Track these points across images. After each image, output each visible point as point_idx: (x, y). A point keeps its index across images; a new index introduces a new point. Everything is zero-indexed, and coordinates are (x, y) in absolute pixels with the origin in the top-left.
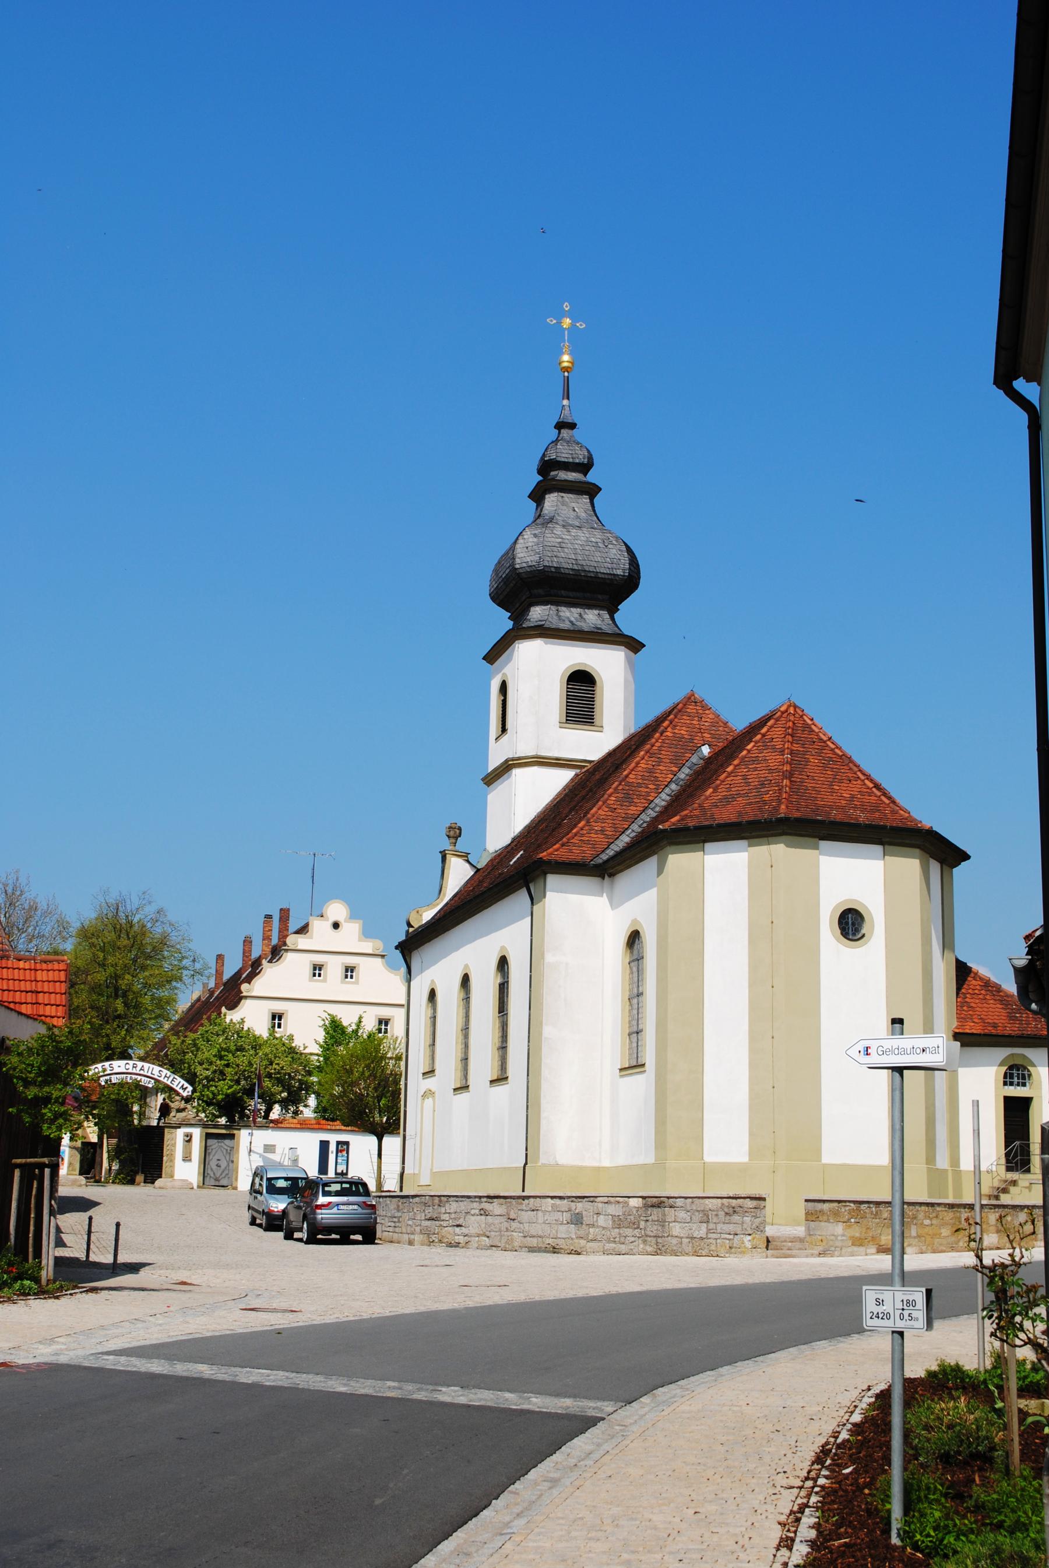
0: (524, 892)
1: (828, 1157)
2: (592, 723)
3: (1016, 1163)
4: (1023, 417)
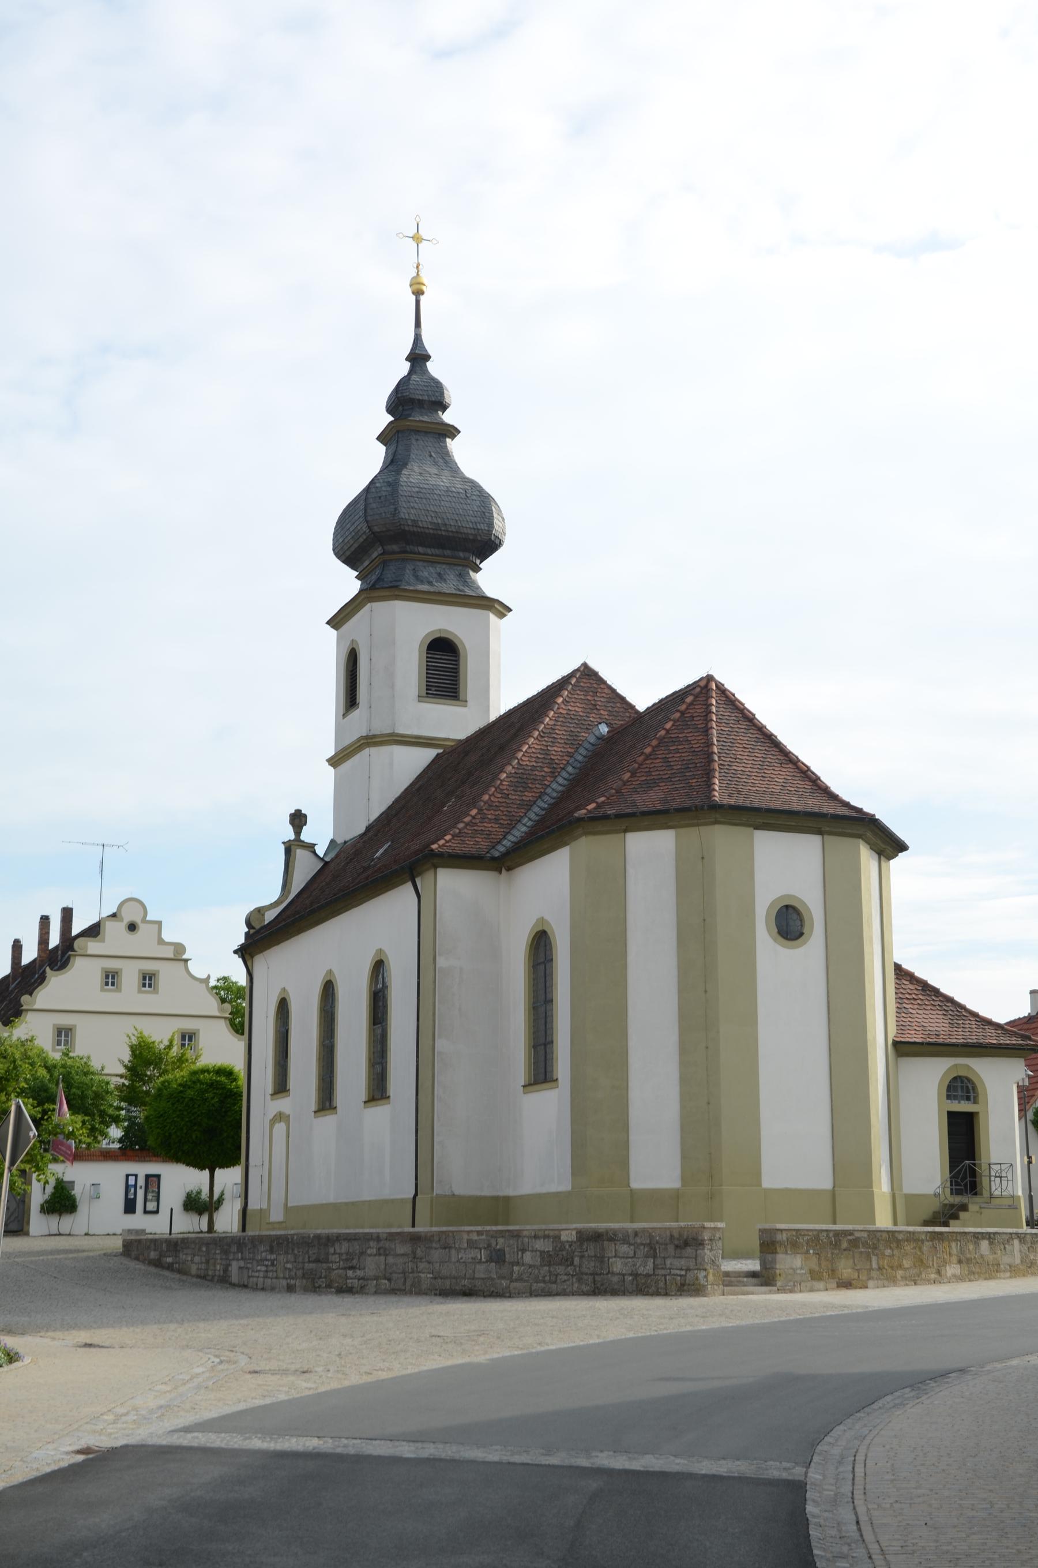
0: (408, 887)
1: (769, 1181)
2: (458, 700)
3: (965, 1185)
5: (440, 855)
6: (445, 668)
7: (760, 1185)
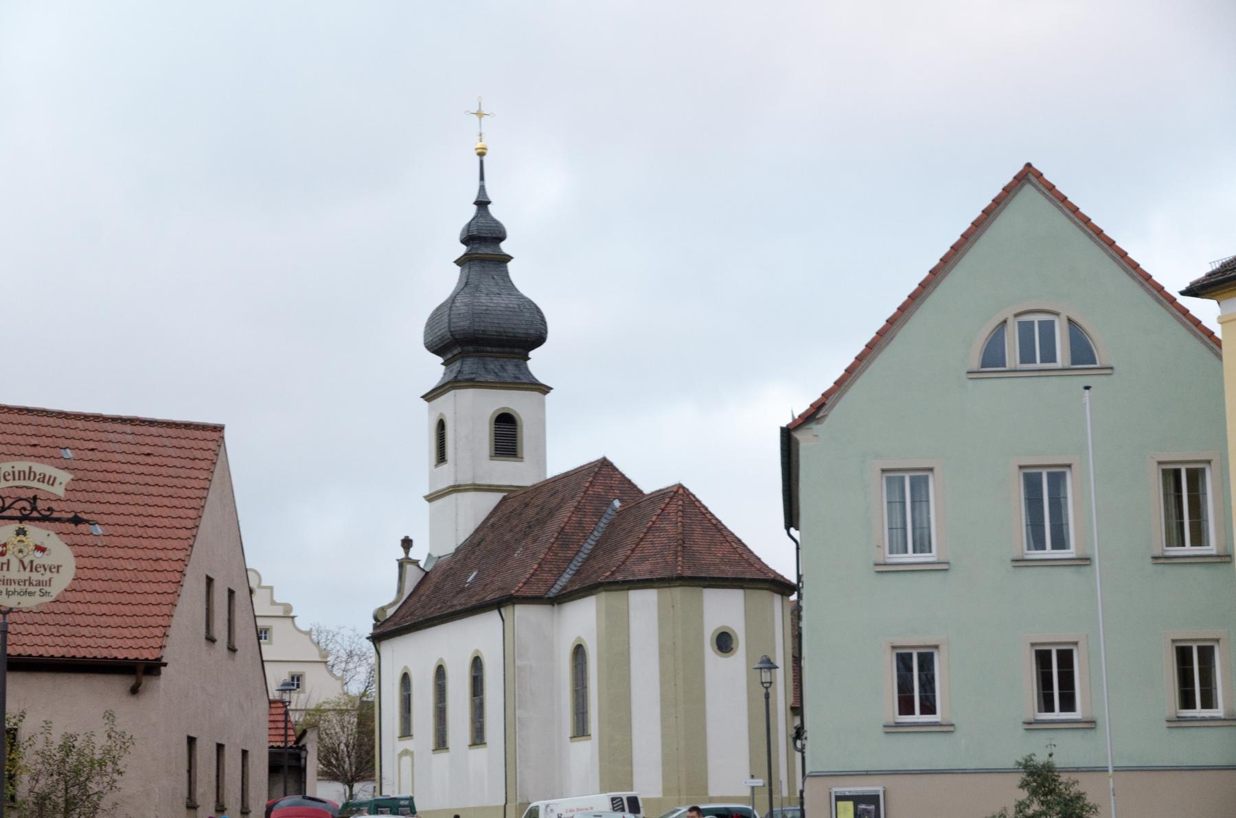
4: (794, 544)
5: (517, 598)
6: (506, 435)
7: (706, 794)
